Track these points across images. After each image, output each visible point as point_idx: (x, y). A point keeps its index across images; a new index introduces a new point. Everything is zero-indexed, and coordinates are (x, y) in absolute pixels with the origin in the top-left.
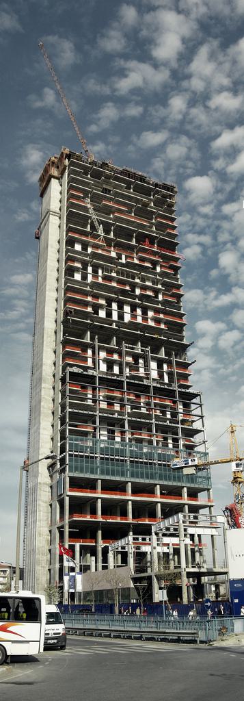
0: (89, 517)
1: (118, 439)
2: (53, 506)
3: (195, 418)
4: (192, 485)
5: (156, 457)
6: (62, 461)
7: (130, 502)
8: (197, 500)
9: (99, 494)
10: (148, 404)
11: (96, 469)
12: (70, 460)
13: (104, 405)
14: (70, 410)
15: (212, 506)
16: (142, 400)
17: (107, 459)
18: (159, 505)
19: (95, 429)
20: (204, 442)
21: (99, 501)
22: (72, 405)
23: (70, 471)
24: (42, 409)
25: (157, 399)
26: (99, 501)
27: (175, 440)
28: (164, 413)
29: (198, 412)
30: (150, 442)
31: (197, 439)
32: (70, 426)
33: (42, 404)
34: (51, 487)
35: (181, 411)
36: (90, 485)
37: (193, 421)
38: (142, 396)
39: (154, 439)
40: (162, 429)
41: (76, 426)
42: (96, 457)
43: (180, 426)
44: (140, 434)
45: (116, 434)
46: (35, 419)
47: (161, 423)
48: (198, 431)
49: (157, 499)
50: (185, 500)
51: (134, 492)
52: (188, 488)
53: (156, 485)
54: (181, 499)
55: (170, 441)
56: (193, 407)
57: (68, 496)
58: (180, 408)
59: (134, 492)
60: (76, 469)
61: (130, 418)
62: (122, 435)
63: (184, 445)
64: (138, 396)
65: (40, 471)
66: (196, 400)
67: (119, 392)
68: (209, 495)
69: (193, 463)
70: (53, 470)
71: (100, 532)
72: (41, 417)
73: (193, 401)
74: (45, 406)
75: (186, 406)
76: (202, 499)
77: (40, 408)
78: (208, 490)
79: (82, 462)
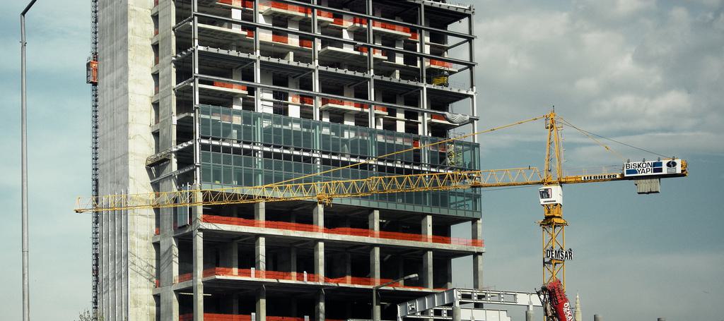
0: (235, 270)
1: (294, 112)
2: (163, 248)
3: (454, 68)
4: (444, 212)
5: (318, 145)
6: (185, 158)
7: (321, 245)
8: (449, 242)
9: (261, 228)
10: (359, 35)
11: (256, 175)
12: (204, 158)
13: (265, 36)
14: (201, 48)
15: (480, 254)
16: (347, 24)
17: (278, 156)
18: (377, 250)
19: (251, 90)
20: (472, 121)
21: (262, 241)
22: (206, 38)
23: (205, 179)
24: (130, 36)
25: (324, 13)
26: (262, 241)
27: (411, 115)
28: (391, 55)
29: (462, 53)
30: (361, 120)
31: (456, 112)
32: (201, 82)
33: (131, 24)
34: (157, 210)
35: (427, 50)
36: (246, 212)
37: (451, 73)
38: (344, 17)
39: (372, 112)
40: (388, 94)
41: (211, 83)
42: (256, 151)
43: (425, 86)
44: (342, 102)
45: (290, 99)
46: (113, 54)
47: (213, 50)
48: (460, 97)
49: (374, 238)
50: (427, 241)
51: (331, 224)
52: (435, 217)
53: (372, 210)
54: (419, 239)
55: (400, 116)
56: (451, 41)
57: (200, 230)
58: (425, 46)
59: (331, 224)
60: (217, 177)
61: (323, 68)
62: (302, 101)
63: (432, 127)
64: (338, 17)
65: (131, 174)
66: (460, 27)
67: (402, 28)
68: (475, 232)
69: (672, 171)
70: (158, 175)
71: (263, 302)
72: (130, 55)
73: (452, 27)
74: (138, 30)
75: (438, 39)
76: (460, 237)
77: (126, 34)
78: (474, 221)
79: (227, 161)
